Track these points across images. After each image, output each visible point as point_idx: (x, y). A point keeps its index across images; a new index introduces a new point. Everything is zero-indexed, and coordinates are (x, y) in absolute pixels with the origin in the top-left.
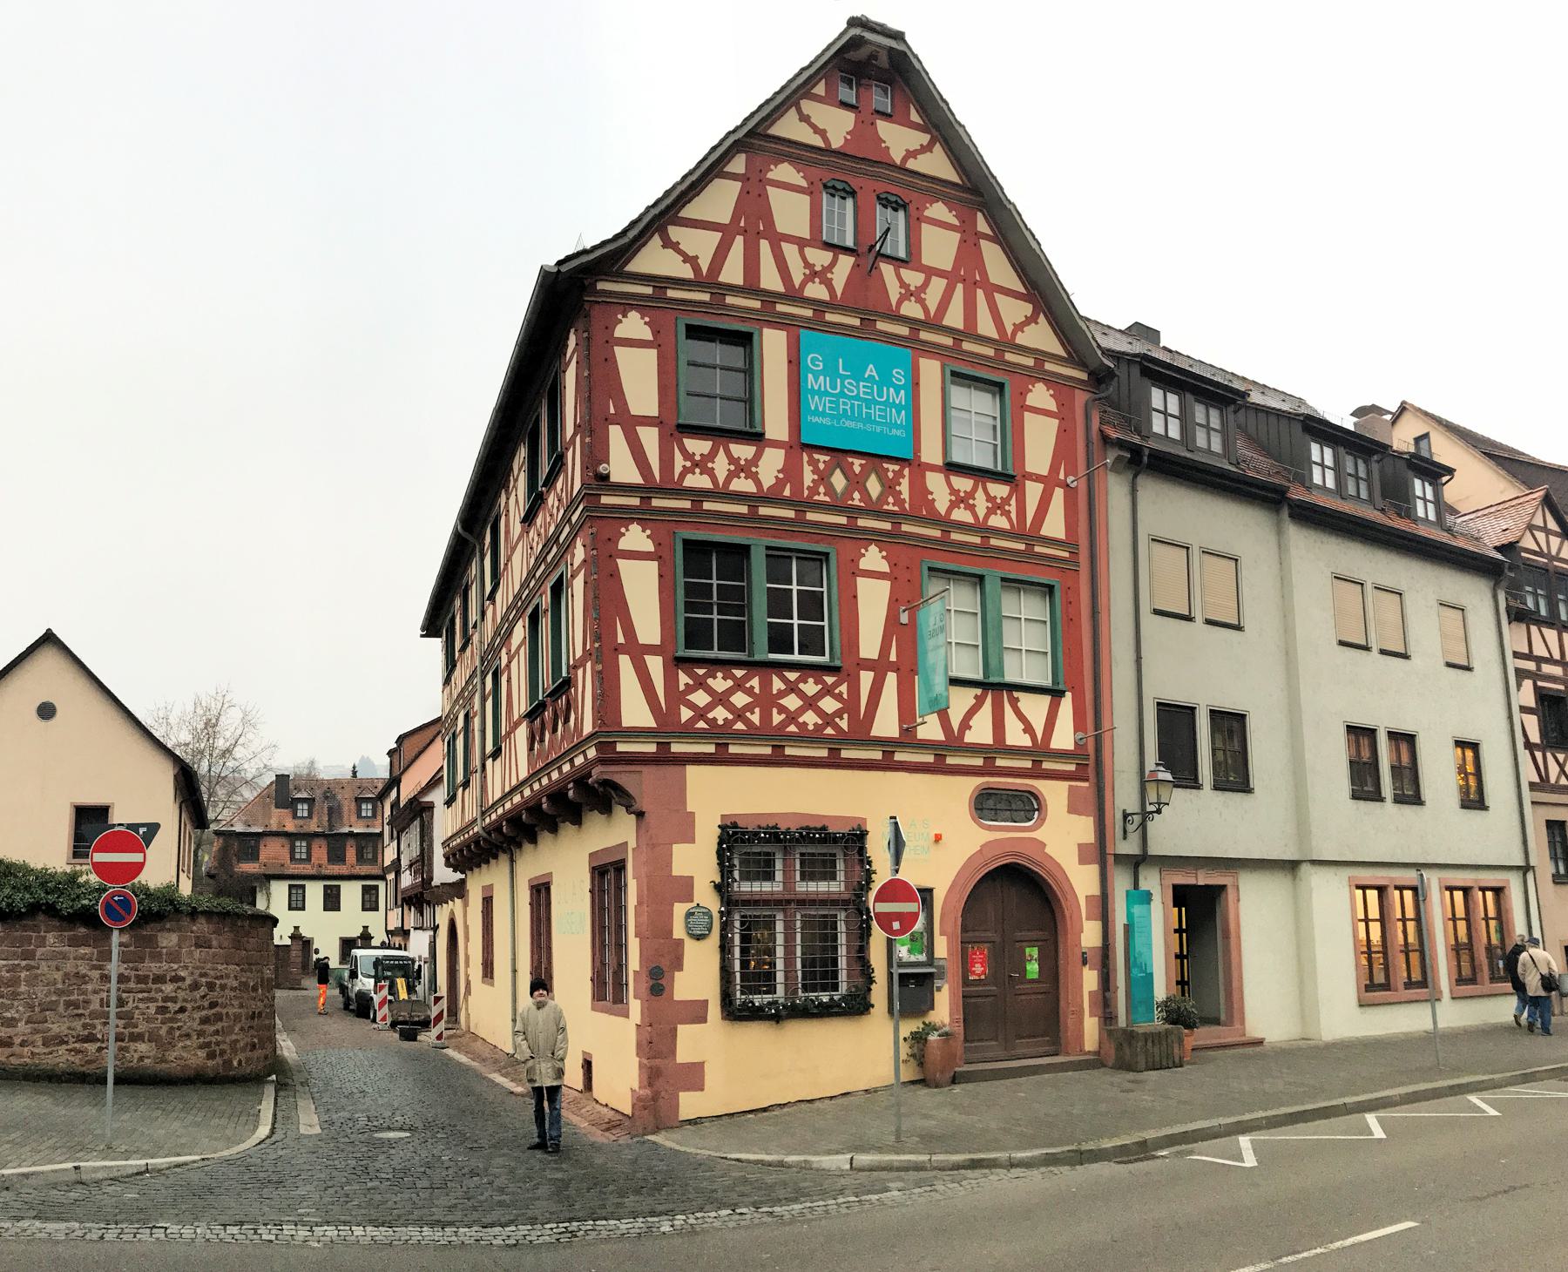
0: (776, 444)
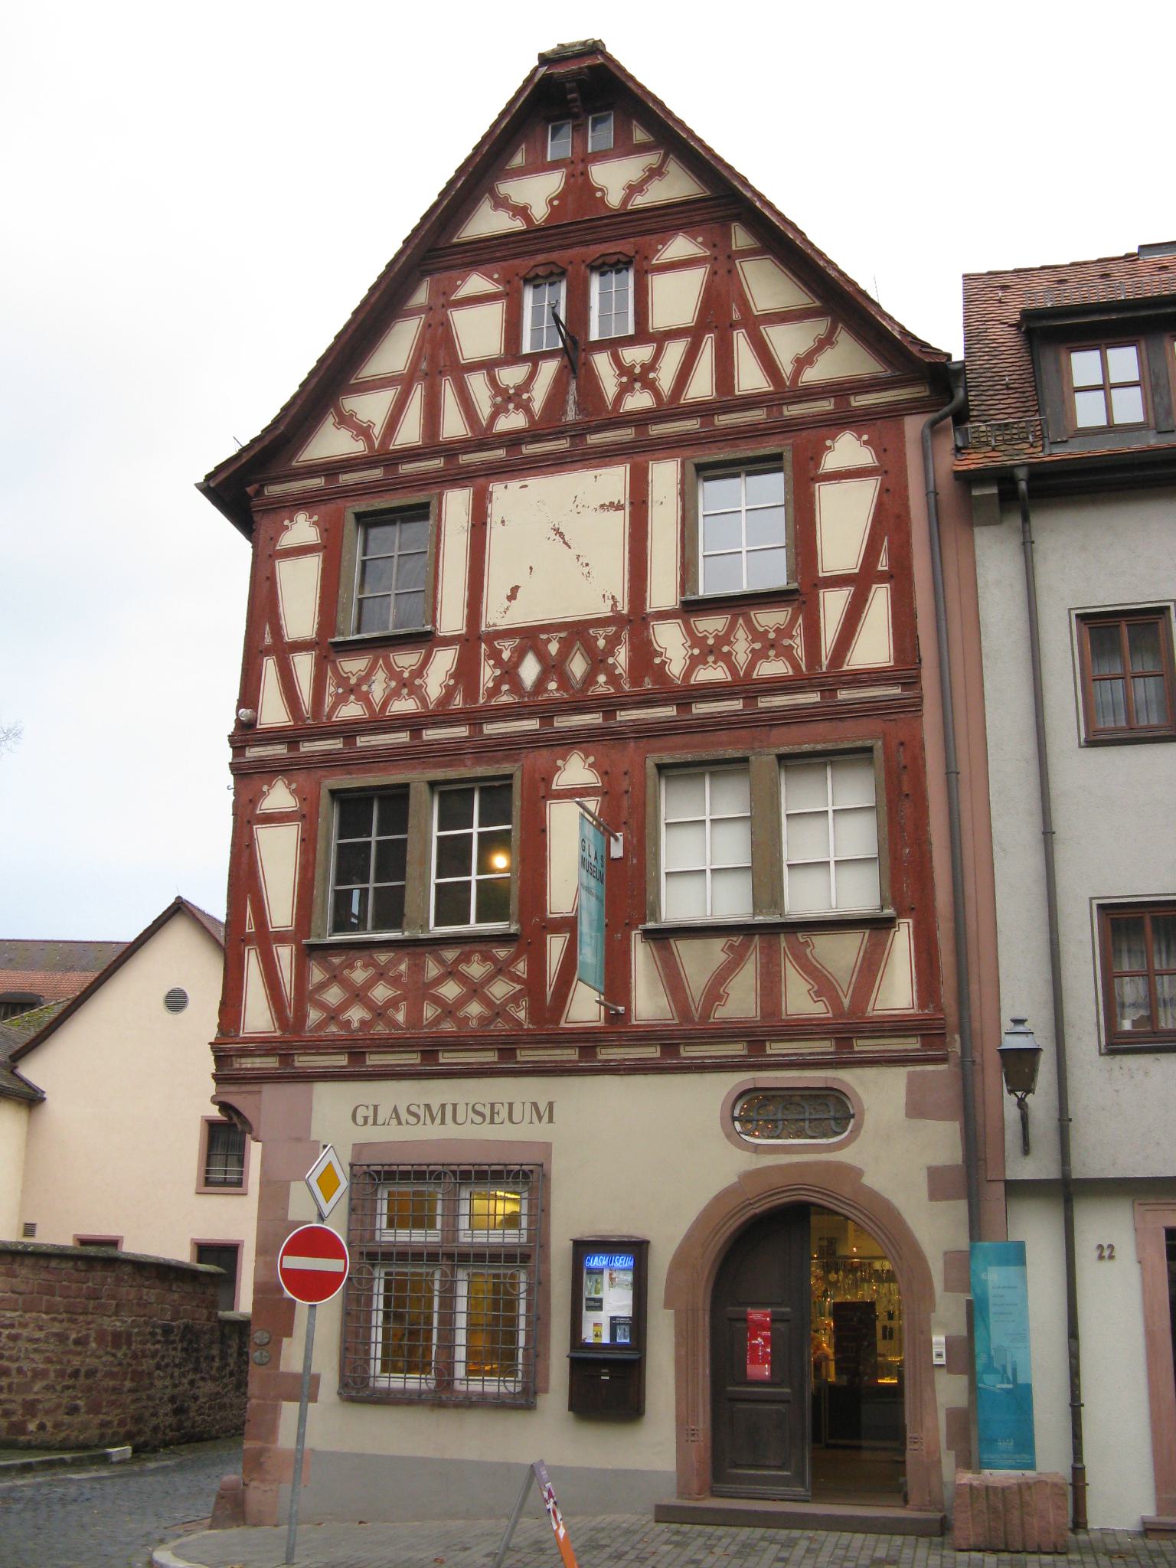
0: (663, 615)
